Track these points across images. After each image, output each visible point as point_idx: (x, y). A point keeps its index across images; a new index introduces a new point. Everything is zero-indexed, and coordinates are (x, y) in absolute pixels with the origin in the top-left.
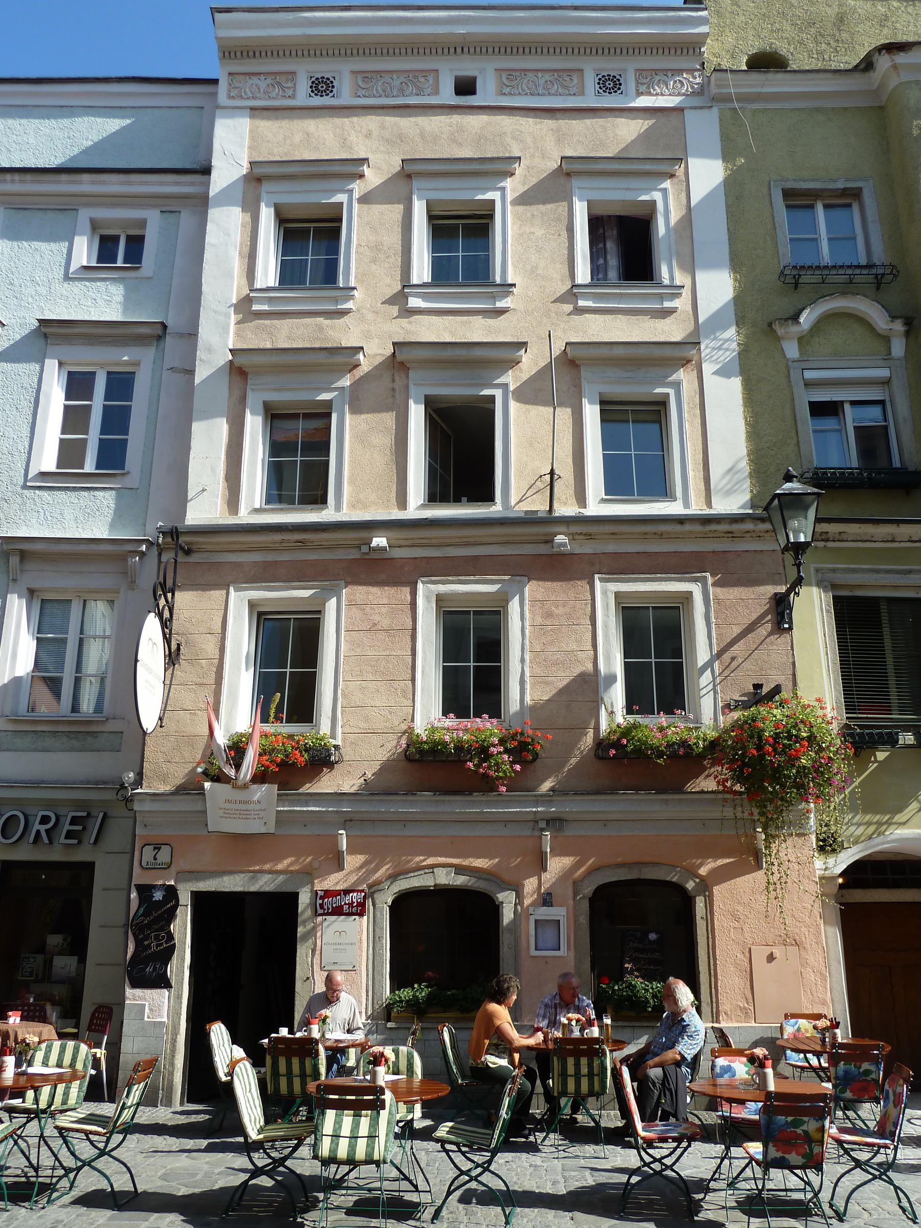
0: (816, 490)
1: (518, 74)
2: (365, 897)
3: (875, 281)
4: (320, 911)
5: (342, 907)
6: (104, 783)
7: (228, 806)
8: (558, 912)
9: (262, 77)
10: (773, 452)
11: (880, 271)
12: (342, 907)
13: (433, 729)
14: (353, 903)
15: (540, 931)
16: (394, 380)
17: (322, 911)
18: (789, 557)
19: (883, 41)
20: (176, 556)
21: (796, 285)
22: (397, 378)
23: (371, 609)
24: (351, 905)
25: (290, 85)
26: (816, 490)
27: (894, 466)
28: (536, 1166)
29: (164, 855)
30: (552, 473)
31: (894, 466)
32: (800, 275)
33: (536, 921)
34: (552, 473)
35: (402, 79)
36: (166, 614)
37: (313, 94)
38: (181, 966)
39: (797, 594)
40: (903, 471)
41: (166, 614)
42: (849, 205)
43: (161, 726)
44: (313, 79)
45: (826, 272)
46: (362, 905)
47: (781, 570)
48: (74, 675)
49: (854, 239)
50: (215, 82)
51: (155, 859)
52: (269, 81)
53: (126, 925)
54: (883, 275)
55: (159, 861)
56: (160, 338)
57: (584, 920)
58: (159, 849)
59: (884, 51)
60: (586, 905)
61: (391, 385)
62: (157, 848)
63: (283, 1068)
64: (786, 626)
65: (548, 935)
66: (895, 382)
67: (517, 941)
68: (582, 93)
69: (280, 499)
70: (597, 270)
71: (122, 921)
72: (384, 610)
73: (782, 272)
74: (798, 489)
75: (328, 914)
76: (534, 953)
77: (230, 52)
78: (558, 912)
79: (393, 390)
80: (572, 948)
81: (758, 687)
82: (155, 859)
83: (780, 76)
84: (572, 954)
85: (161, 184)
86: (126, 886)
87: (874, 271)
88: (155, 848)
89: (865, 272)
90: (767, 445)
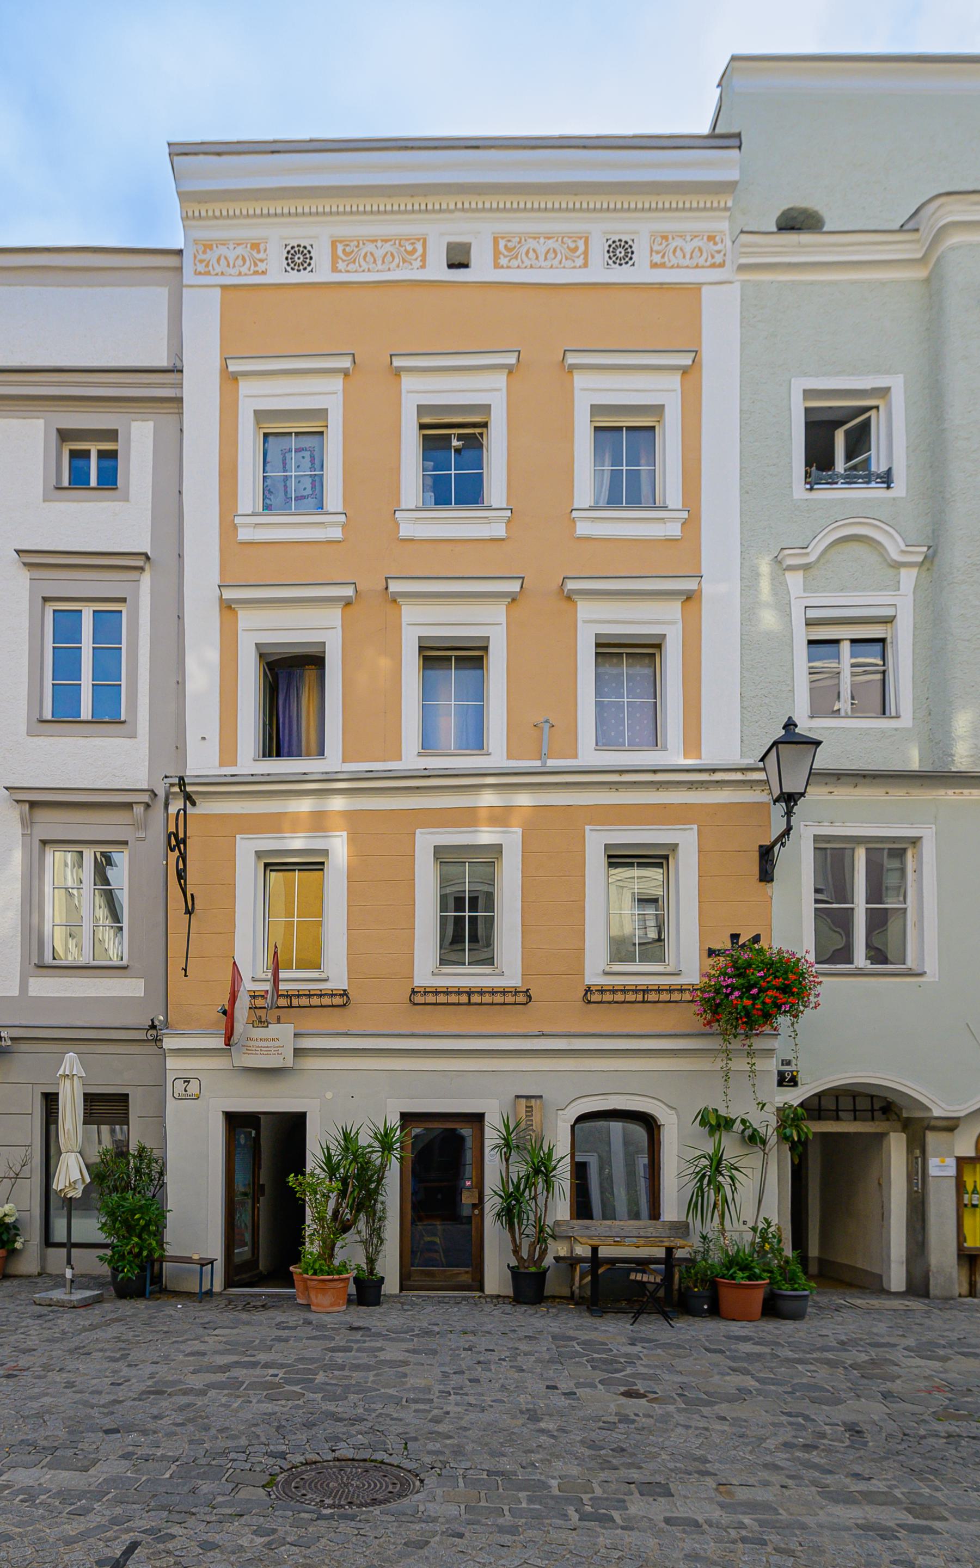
39: (783, 845)
51: (186, 1091)
81: (735, 937)
82: (186, 1091)
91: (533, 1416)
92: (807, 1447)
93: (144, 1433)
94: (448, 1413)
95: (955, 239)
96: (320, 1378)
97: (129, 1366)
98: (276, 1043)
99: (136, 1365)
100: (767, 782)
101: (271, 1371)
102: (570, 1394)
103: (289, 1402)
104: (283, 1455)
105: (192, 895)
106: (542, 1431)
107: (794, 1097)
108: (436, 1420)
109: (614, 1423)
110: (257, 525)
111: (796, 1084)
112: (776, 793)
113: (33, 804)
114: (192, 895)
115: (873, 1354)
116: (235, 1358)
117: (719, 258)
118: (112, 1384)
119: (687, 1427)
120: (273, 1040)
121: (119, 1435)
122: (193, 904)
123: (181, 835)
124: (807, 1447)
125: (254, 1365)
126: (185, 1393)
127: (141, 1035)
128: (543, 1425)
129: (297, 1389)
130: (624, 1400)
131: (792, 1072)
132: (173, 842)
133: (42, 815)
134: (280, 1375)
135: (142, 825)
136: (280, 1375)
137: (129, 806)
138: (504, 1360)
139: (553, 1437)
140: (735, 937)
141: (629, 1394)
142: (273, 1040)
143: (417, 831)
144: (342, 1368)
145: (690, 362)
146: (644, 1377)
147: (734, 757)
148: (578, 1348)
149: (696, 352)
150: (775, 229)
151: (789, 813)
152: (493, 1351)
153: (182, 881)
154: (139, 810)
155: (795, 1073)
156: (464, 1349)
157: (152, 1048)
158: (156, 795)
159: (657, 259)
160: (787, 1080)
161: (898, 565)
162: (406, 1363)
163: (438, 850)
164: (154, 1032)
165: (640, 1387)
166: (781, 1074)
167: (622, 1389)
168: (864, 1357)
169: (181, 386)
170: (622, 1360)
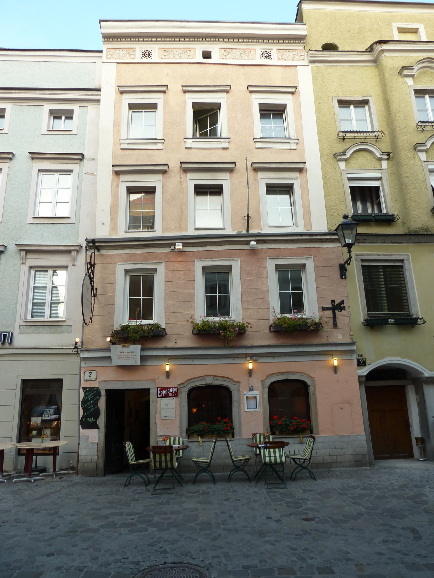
0: (356, 222)
1: (228, 50)
2: (177, 390)
3: (375, 138)
4: (159, 396)
5: (168, 394)
6: (65, 346)
7: (120, 354)
8: (255, 393)
9: (121, 50)
10: (336, 207)
11: (377, 134)
12: (168, 394)
13: (203, 322)
14: (173, 392)
15: (248, 401)
16: (181, 178)
17: (160, 396)
18: (346, 249)
19: (379, 40)
20: (95, 251)
21: (344, 139)
22: (182, 177)
23: (176, 272)
24: (172, 393)
25: (132, 53)
26: (356, 222)
27: (383, 213)
28: (256, 492)
29: (94, 375)
30: (248, 216)
31: (383, 213)
32: (345, 135)
33: (247, 397)
34: (248, 216)
35: (180, 52)
36: (92, 276)
37: (143, 58)
38: (101, 421)
39: (349, 264)
40: (387, 215)
41: (92, 276)
42: (364, 107)
43: (91, 322)
44: (143, 51)
45: (356, 134)
46: (177, 393)
47: (341, 255)
48: (50, 302)
49: (366, 120)
50: (101, 52)
51: (90, 377)
52: (124, 52)
53: (79, 404)
54: (378, 135)
55: (91, 378)
56: (81, 160)
57: (266, 396)
58: (91, 373)
59: (378, 44)
60: (266, 390)
61: (180, 180)
62: (91, 372)
63: (158, 459)
64: (344, 277)
65: (252, 402)
66: (384, 179)
67: (239, 404)
68: (256, 59)
69: (135, 227)
70: (195, 134)
71: (77, 403)
72: (181, 273)
73: (338, 134)
74: (349, 222)
75: (163, 397)
76: (246, 410)
77: (108, 38)
78: (255, 393)
79: (181, 182)
80: (262, 407)
81: (333, 302)
82: (90, 377)
83: (336, 53)
84: (262, 410)
85: (93, 95)
86: (78, 388)
87: (375, 134)
88: (90, 373)
89: (371, 134)
90: (334, 204)
91: (262, 534)
92: (394, 541)
93: (68, 554)
94: (220, 535)
95: (386, 54)
96: (156, 519)
97: (59, 517)
98: (132, 354)
99: (63, 517)
100: (210, 116)
101: (132, 517)
102: (278, 521)
103: (141, 533)
104: (138, 563)
105: (96, 288)
106: (267, 542)
107: (365, 371)
108: (215, 539)
109: (301, 535)
110: (128, 143)
111: (365, 365)
112: (343, 244)
113: (27, 252)
114: (96, 288)
115: (416, 491)
116: (112, 511)
117: (302, 57)
118: (51, 528)
119: (336, 535)
120: (131, 352)
121: (54, 557)
122: (96, 292)
123: (92, 263)
124: (394, 541)
125: (121, 514)
126: (88, 531)
127: (70, 351)
128: (267, 539)
129: (144, 526)
130: (305, 522)
131: (363, 359)
132: (89, 266)
133: (29, 256)
134: (135, 519)
135: (74, 260)
136: (135, 519)
137: (69, 252)
138: (244, 505)
139: (273, 544)
140: (333, 302)
141: (307, 520)
142: (131, 352)
143: (195, 260)
144: (166, 514)
145: (295, 90)
146: (311, 510)
147: (324, 228)
148: (279, 496)
149: (297, 87)
150: (322, 50)
151: (349, 252)
152: (239, 500)
153: (92, 283)
154: (74, 253)
155: (364, 360)
156: (225, 500)
157: (75, 358)
158: (82, 247)
159: (280, 57)
160: (361, 363)
161: (380, 160)
162: (197, 509)
163: (204, 268)
164: (76, 350)
165: (310, 516)
166: (358, 361)
167: (303, 517)
168: (411, 493)
169: (100, 95)
170: (301, 501)
